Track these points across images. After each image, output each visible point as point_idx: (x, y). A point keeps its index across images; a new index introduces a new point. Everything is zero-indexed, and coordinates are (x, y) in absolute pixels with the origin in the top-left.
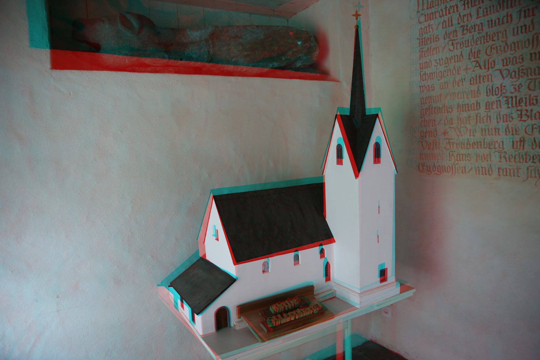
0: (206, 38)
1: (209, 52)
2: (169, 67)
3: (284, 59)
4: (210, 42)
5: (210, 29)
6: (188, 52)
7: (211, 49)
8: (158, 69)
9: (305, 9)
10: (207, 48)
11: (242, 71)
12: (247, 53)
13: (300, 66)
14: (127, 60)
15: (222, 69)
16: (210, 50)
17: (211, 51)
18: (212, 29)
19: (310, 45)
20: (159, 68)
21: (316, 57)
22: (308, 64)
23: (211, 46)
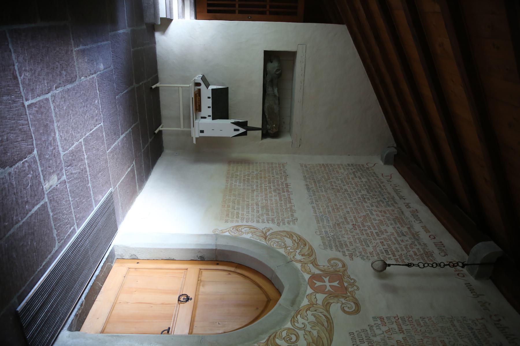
3: (269, 119)
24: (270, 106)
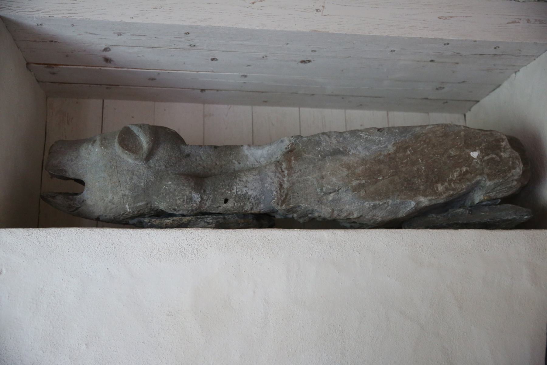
0: (279, 158)
1: (281, 185)
2: (207, 216)
3: (440, 188)
4: (284, 166)
5: (287, 142)
6: (238, 187)
7: (285, 179)
8: (185, 219)
9: (494, 90)
10: (278, 177)
11: (351, 217)
12: (358, 182)
13: (481, 202)
14: (127, 206)
15: (310, 215)
16: (283, 181)
17: (286, 182)
18: (290, 141)
19: (501, 157)
20: (188, 218)
21: (516, 180)
22: (500, 195)
23: (286, 172)
24: (355, 183)
